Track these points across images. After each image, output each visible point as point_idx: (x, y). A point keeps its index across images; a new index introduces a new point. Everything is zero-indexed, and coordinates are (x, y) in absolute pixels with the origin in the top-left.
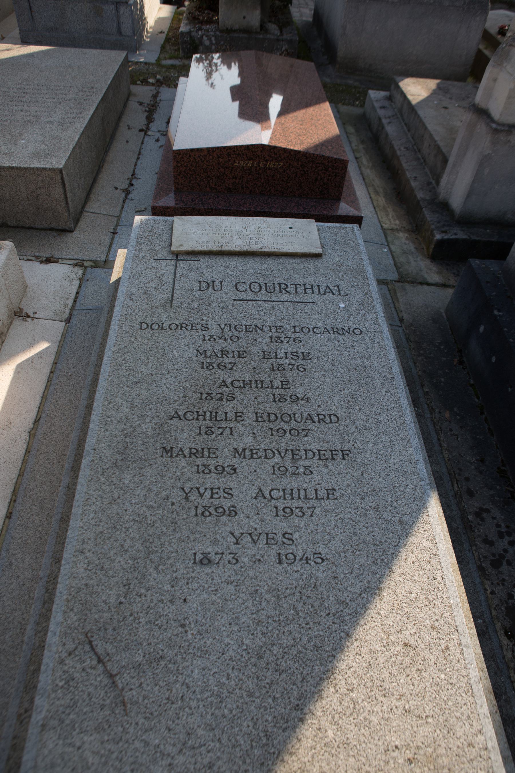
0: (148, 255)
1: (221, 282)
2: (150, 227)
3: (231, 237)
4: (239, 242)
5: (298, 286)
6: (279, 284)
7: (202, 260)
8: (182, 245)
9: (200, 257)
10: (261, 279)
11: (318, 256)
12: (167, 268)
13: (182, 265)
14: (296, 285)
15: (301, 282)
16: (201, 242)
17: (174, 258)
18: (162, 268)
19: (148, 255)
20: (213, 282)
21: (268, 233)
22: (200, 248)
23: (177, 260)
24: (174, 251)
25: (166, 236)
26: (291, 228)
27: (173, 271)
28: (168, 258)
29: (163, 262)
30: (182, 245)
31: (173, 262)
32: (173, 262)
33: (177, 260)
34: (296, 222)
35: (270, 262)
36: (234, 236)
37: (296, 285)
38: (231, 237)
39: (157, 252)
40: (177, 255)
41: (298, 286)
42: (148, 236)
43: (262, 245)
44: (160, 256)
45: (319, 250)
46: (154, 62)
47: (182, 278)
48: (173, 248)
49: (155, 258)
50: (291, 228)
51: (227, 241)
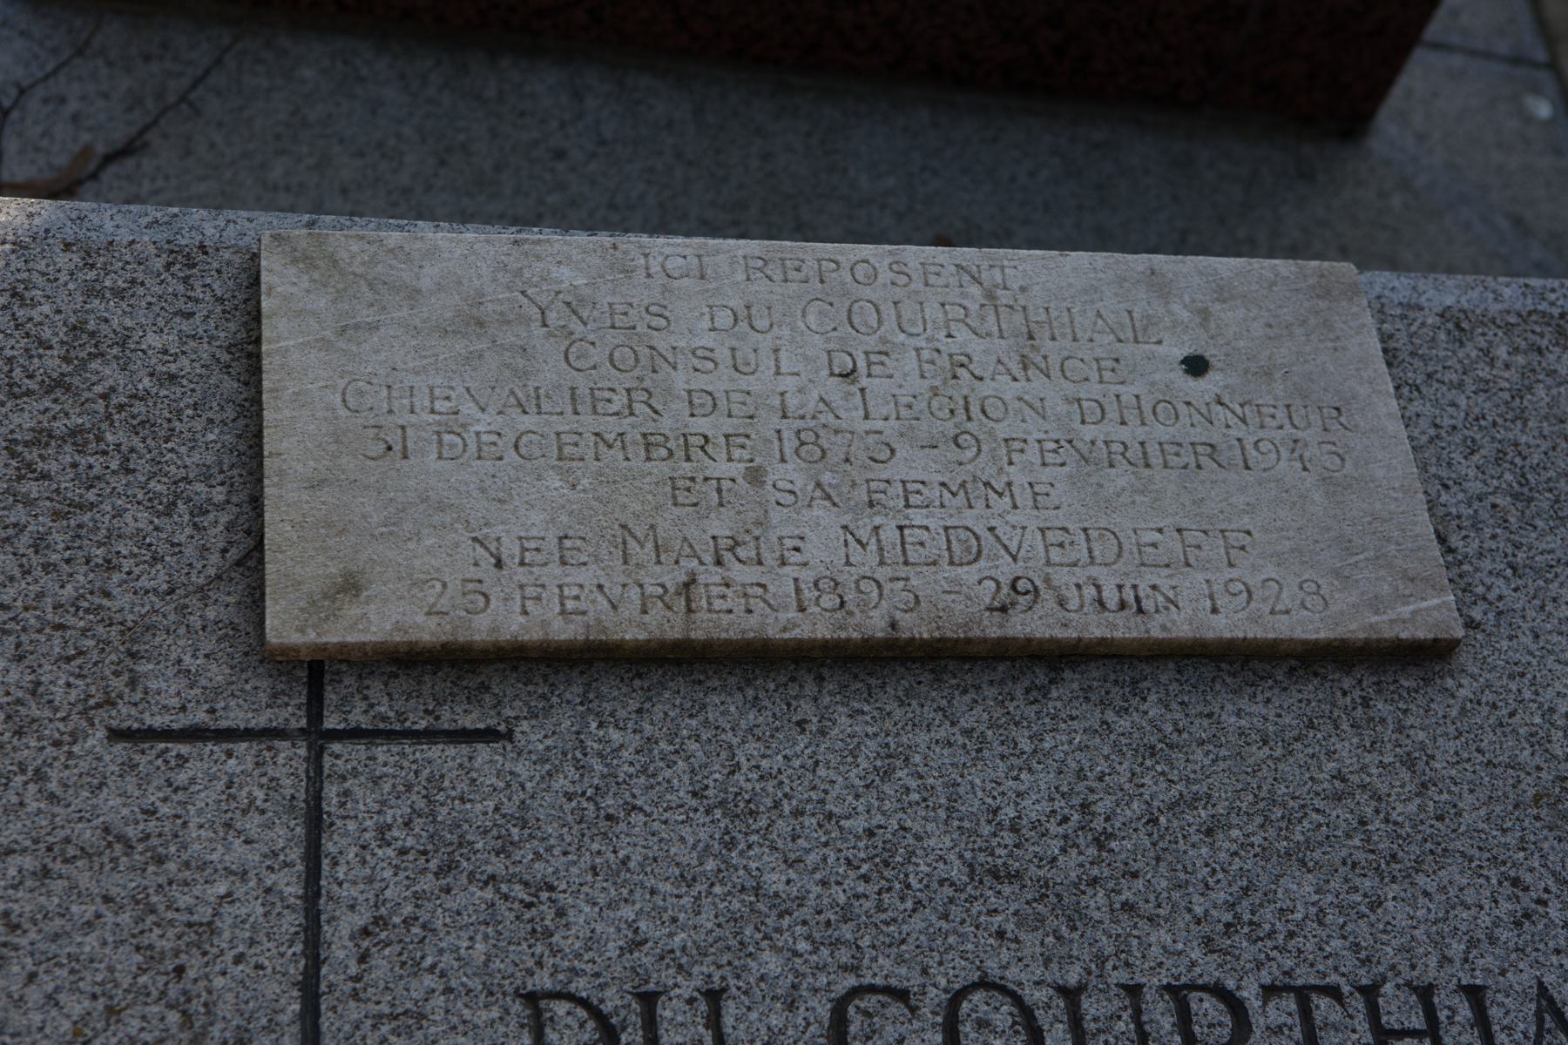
0: (57, 681)
1: (714, 997)
2: (55, 333)
3: (755, 476)
4: (821, 537)
5: (1322, 1004)
6: (1177, 994)
7: (530, 734)
8: (351, 586)
9: (511, 701)
10: (1031, 942)
11: (1426, 657)
12: (227, 819)
13: (368, 786)
14: (1303, 995)
15: (1347, 971)
16: (510, 549)
17: (292, 714)
18: (199, 840)
19: (57, 681)
20: (649, 1000)
21: (1034, 429)
22: (505, 619)
23: (317, 737)
24: (285, 650)
25: (203, 446)
26: (1196, 366)
27: (290, 885)
28: (237, 717)
29: (202, 761)
30: (351, 586)
31: (289, 759)
32: (289, 759)
33: (317, 737)
34: (1223, 293)
35: (1072, 735)
36: (778, 474)
37: (1303, 995)
38: (755, 476)
39: (134, 641)
40: (315, 671)
41: (1322, 1004)
42: (41, 438)
43: (1006, 570)
44: (166, 697)
45: (1427, 612)
46: (272, 637)
47: (381, 967)
48: (285, 624)
49: (123, 715)
50: (1196, 366)
51: (721, 526)
